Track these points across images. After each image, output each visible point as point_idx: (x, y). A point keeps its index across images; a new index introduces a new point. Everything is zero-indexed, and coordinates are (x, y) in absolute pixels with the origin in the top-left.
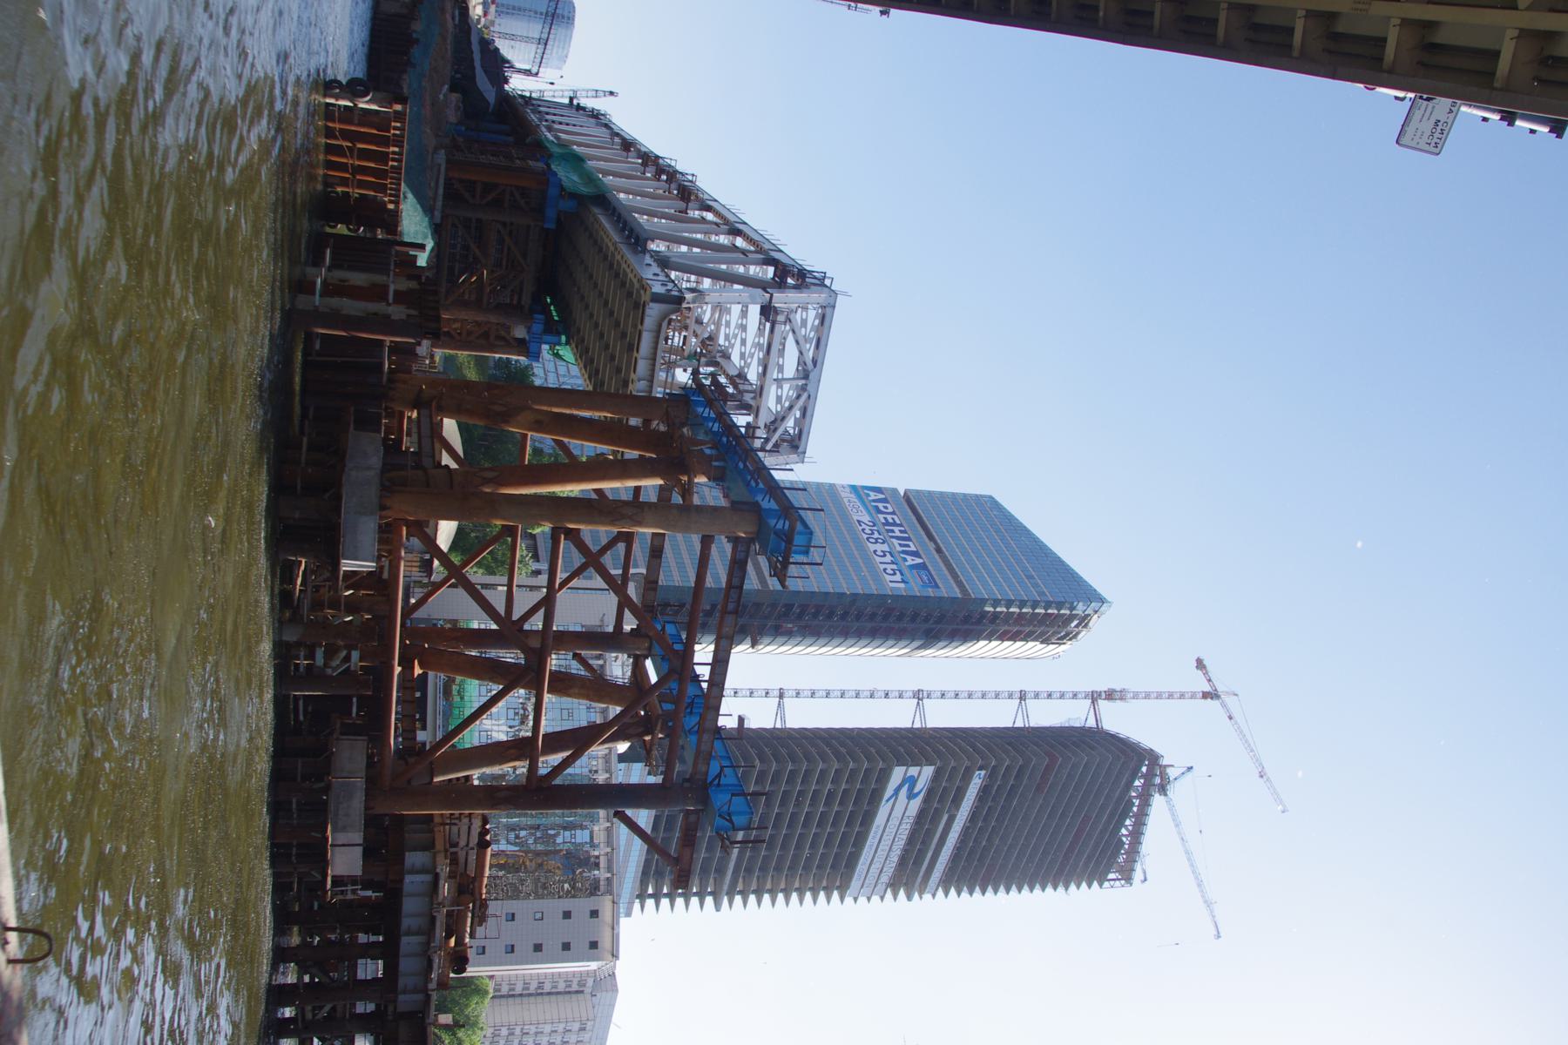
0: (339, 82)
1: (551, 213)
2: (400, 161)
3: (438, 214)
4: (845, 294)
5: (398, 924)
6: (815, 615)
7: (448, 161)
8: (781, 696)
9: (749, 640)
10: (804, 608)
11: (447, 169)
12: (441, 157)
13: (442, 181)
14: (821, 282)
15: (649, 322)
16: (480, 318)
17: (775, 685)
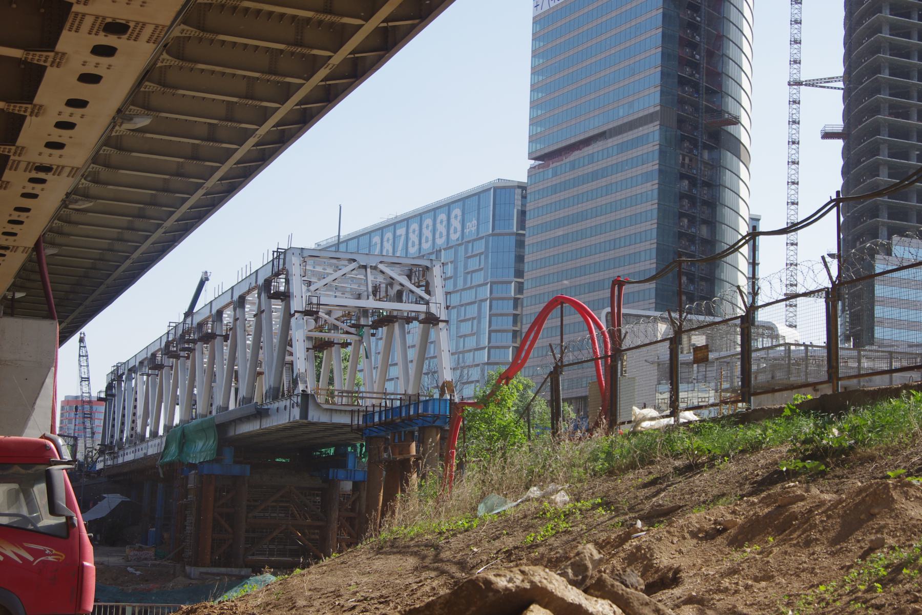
0: (439, 553)
1: (236, 470)
2: (163, 608)
3: (244, 572)
4: (290, 237)
5: (520, 591)
6: (694, 46)
7: (196, 564)
8: (799, 83)
9: (731, 129)
10: (683, 62)
11: (203, 566)
12: (194, 571)
13: (215, 570)
14: (281, 255)
15: (324, 418)
16: (335, 525)
17: (786, 92)
